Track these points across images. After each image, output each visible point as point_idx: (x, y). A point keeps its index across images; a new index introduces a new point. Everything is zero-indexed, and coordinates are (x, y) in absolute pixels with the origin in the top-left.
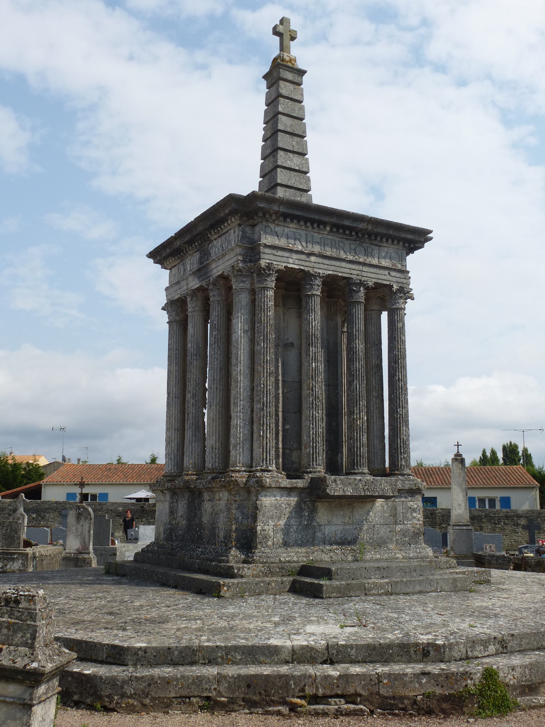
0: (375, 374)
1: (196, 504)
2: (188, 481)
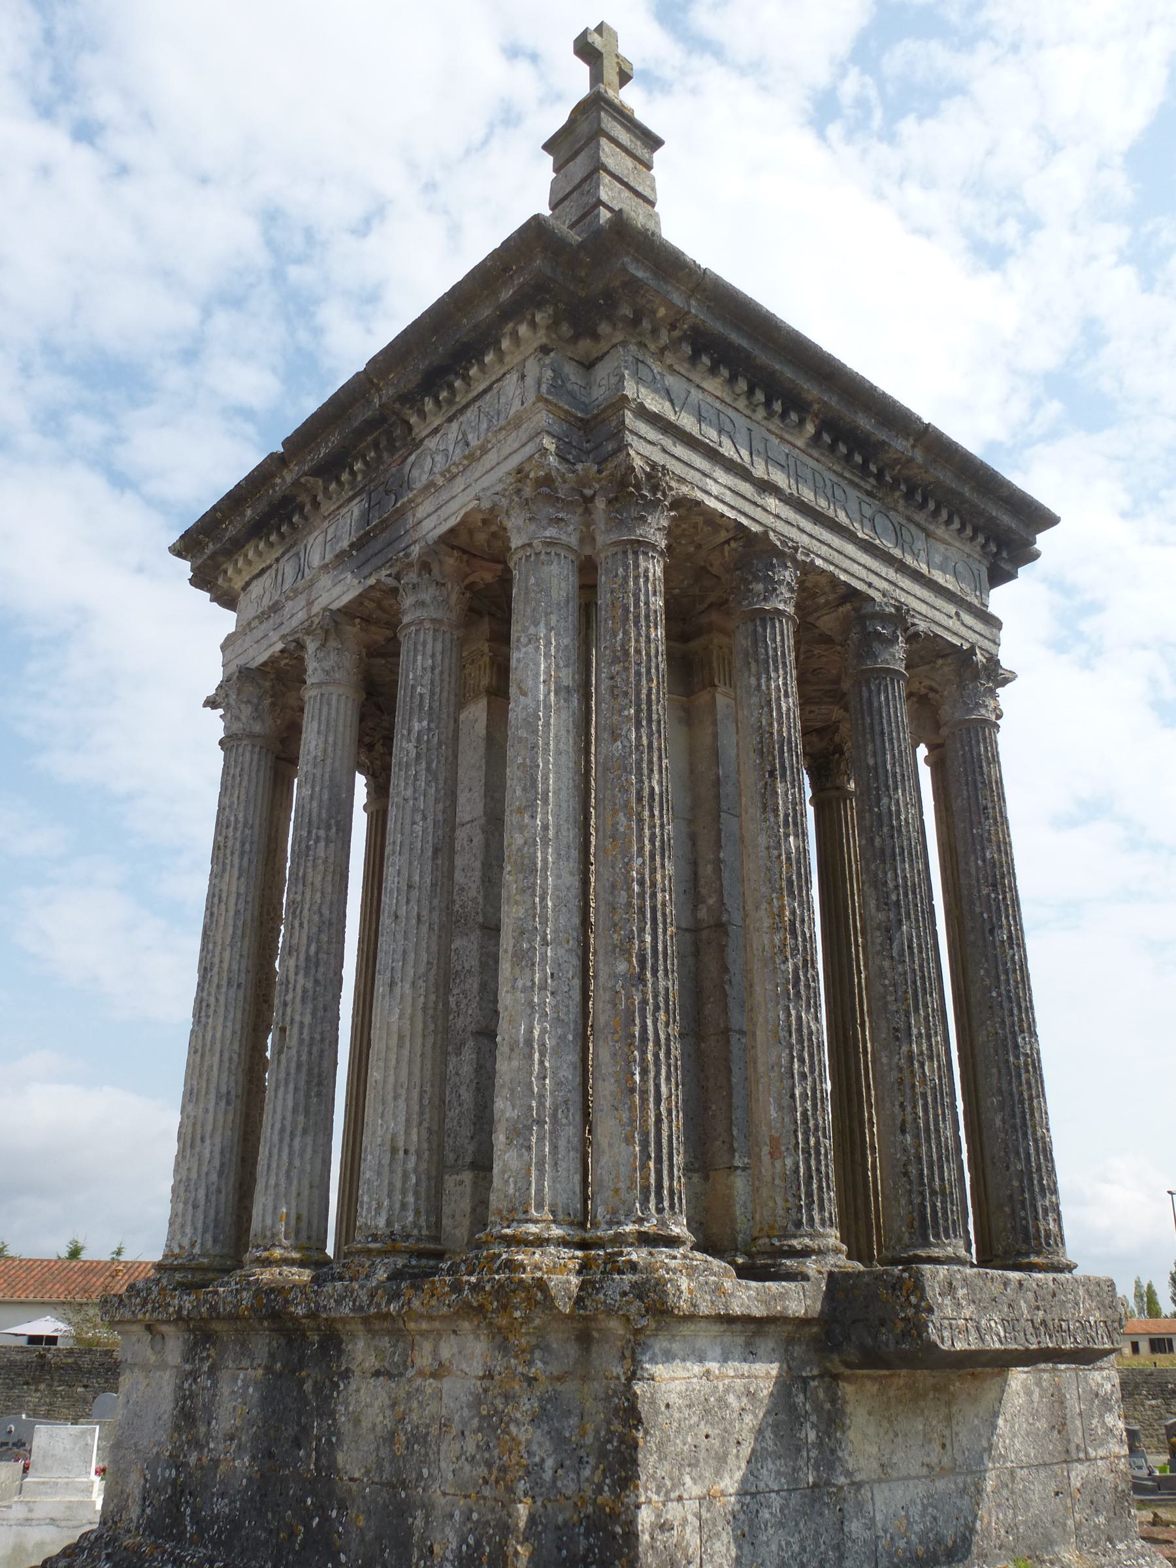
1: (308, 1386)
2: (277, 1290)
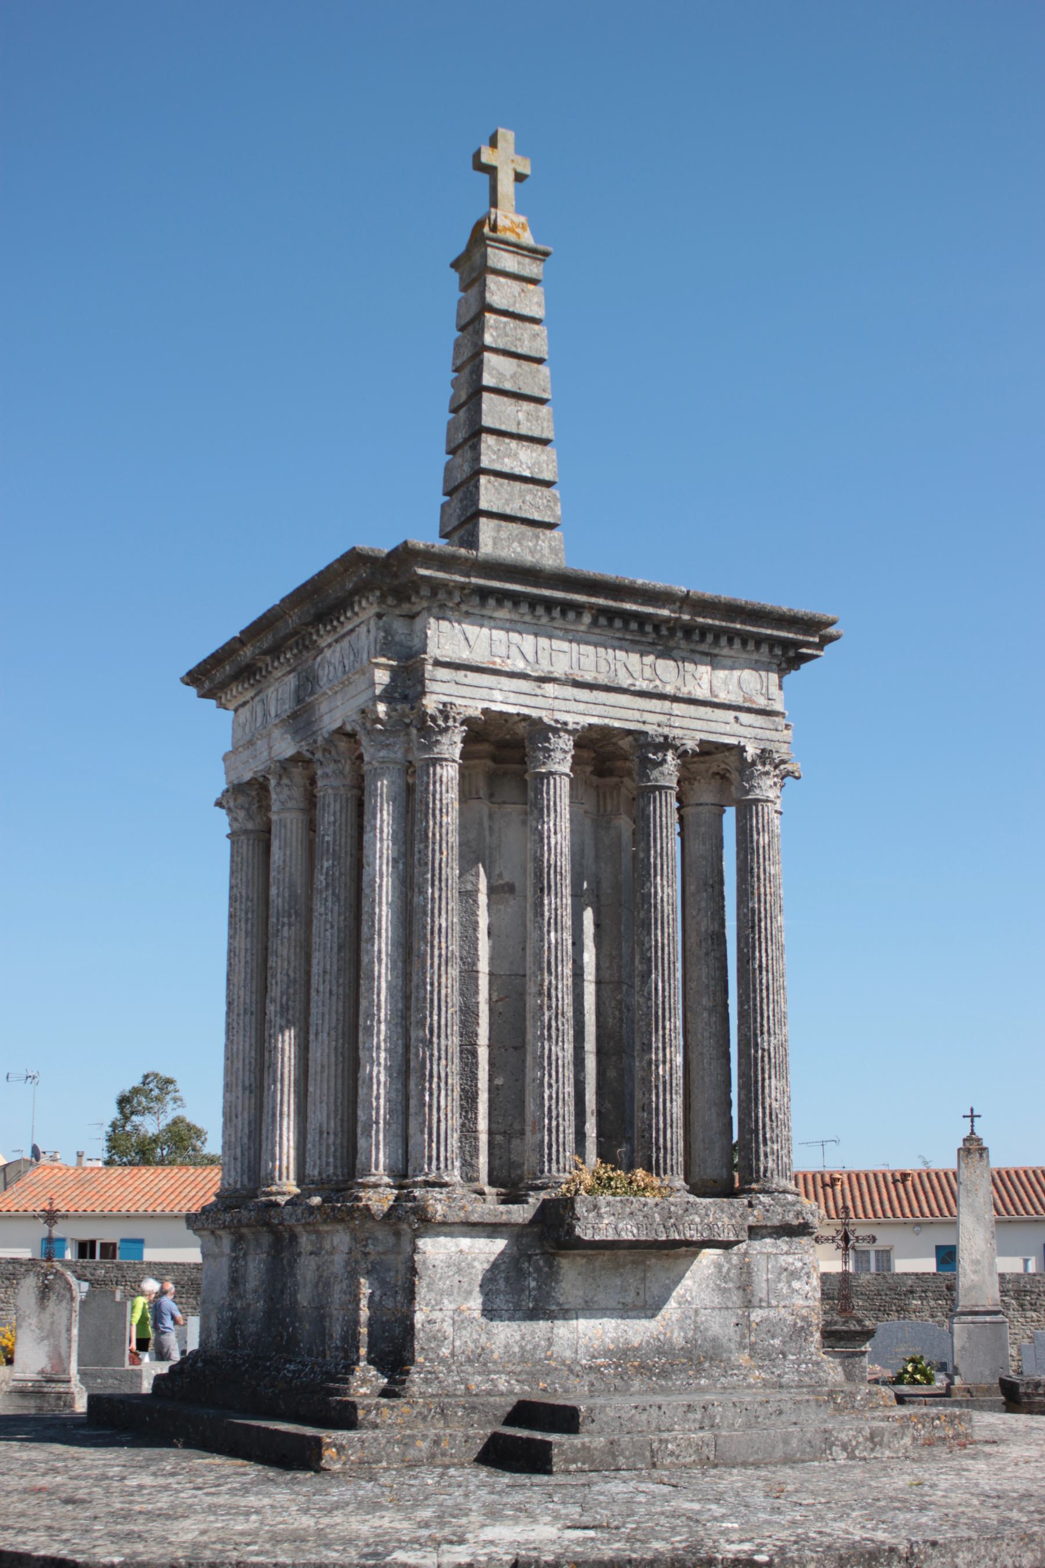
0: (707, 954)
1: (285, 1262)
